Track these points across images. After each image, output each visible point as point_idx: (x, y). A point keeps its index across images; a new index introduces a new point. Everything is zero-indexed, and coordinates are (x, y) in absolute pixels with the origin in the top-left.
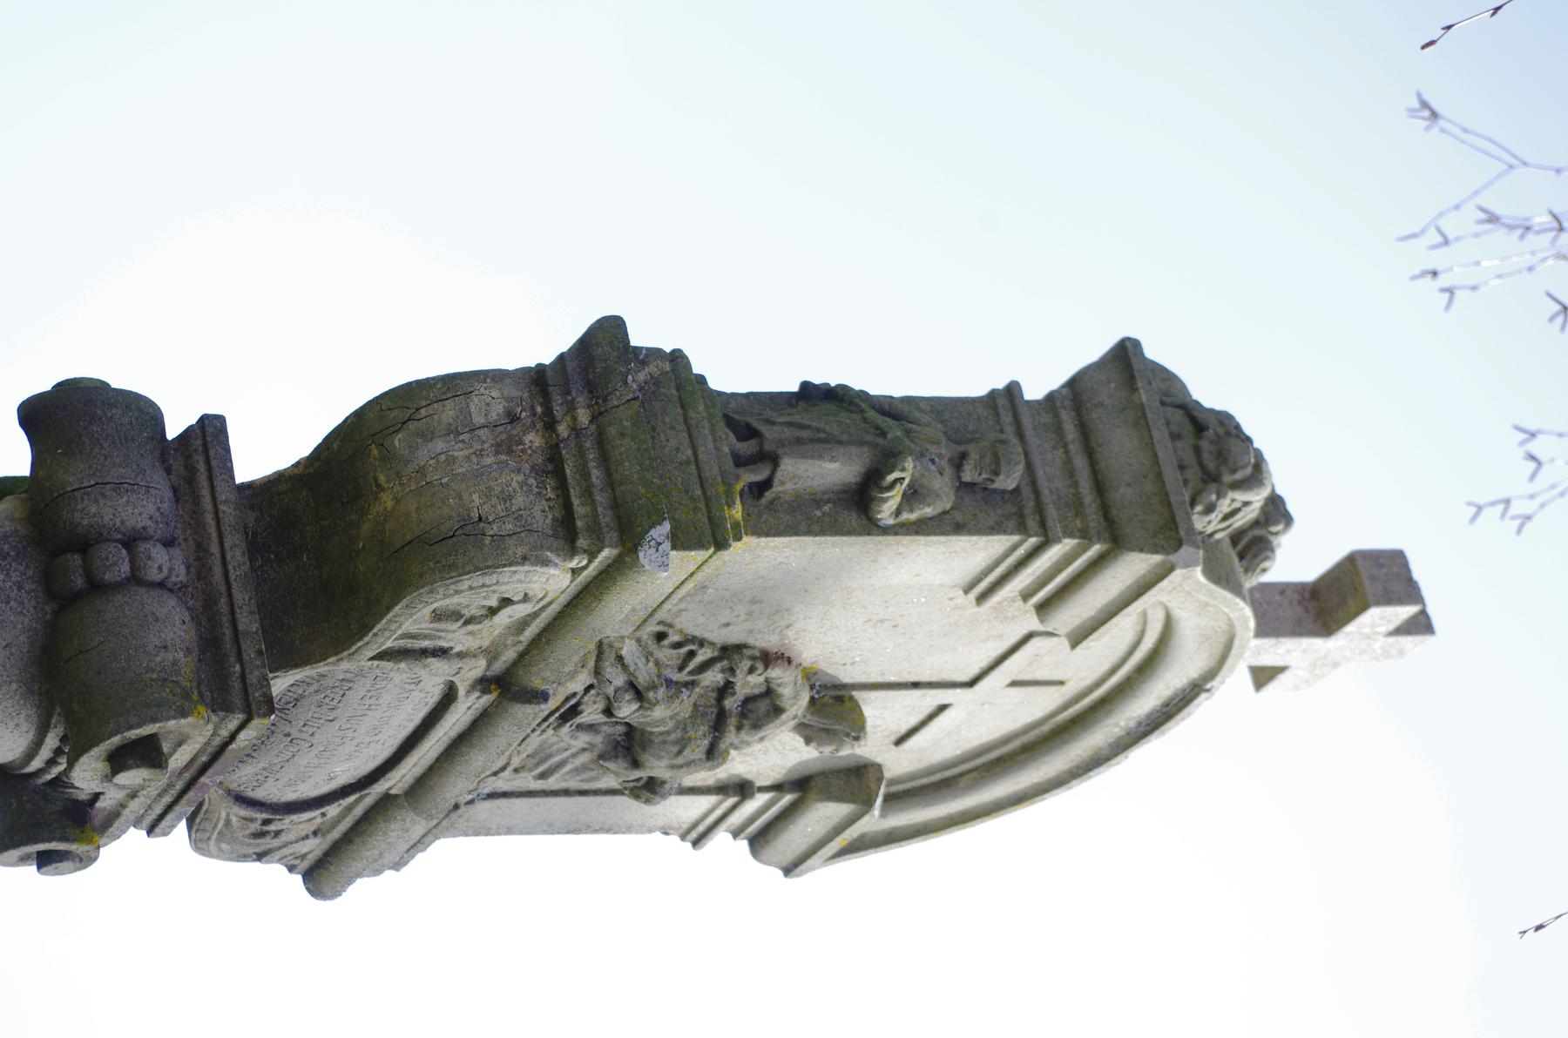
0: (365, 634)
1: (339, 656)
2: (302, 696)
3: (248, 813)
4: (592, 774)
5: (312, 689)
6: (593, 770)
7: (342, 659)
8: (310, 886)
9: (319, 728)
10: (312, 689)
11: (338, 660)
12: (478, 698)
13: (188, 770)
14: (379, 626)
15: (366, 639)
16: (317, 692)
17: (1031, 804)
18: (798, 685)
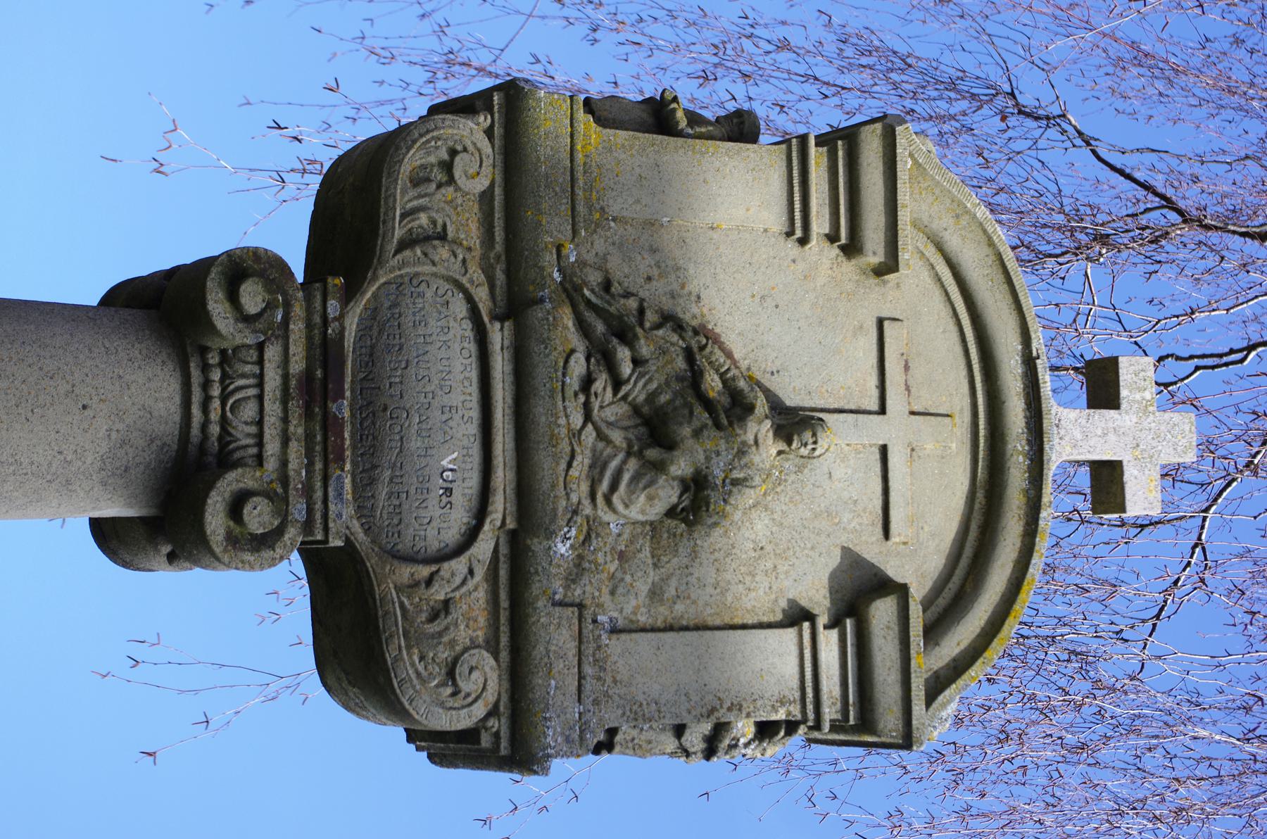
0: (377, 228)
1: (373, 267)
2: (373, 347)
3: (318, 525)
4: (648, 477)
5: (375, 332)
6: (645, 474)
7: (376, 269)
8: (224, 256)
9: (401, 382)
10: (375, 332)
11: (374, 273)
12: (502, 329)
13: (458, 742)
14: (382, 210)
15: (381, 232)
16: (379, 333)
17: (988, 327)
18: (621, 539)
